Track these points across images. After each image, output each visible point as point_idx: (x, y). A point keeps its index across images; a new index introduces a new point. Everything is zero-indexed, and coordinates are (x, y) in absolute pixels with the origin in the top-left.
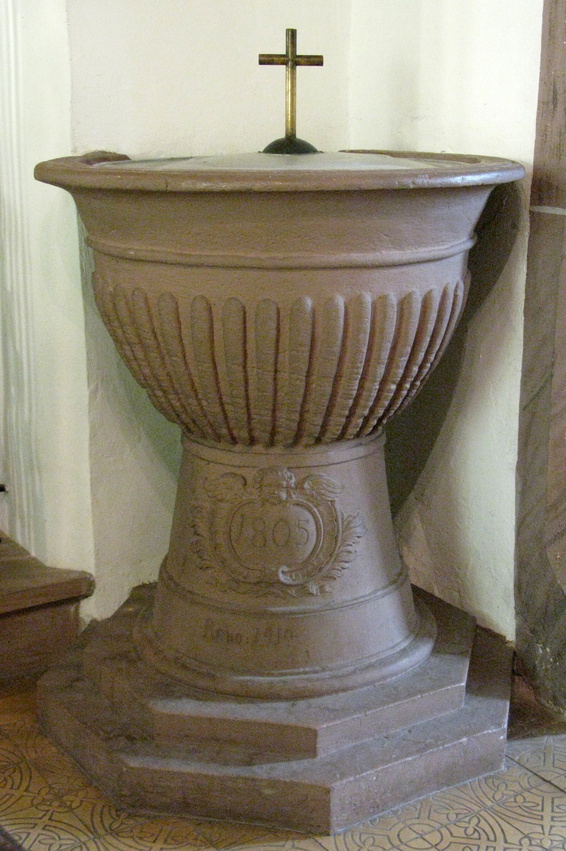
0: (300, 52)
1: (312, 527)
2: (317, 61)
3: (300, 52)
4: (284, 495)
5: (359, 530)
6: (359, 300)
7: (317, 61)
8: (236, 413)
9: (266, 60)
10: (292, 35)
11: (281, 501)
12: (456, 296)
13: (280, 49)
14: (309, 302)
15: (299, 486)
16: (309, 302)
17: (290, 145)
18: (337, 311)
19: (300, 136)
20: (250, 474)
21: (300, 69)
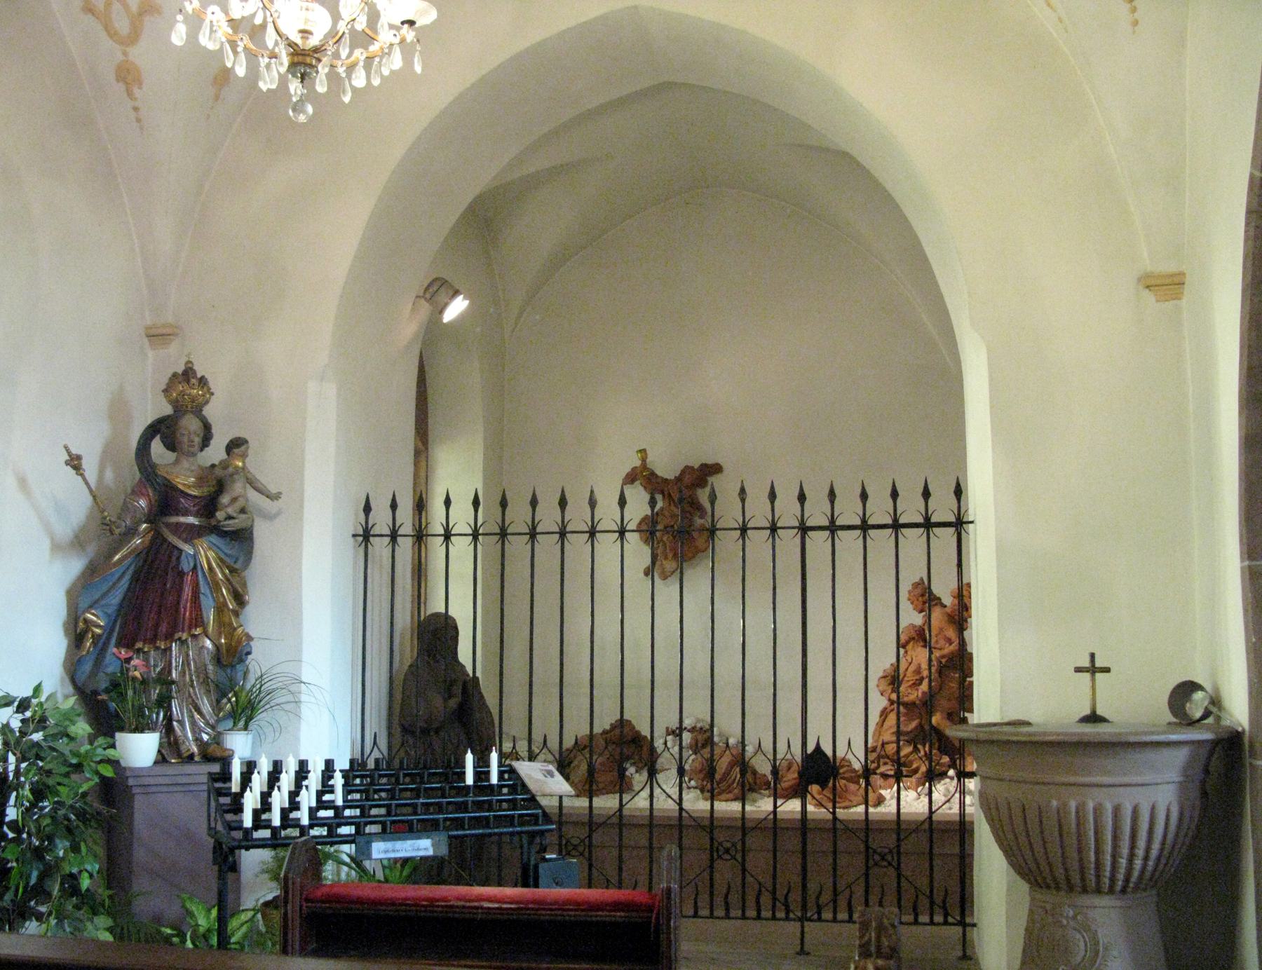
0: (1098, 665)
1: (1082, 944)
2: (1107, 670)
3: (1098, 665)
4: (1065, 922)
5: (1115, 953)
6: (1065, 805)
7: (1107, 670)
8: (1060, 872)
9: (1078, 670)
10: (1092, 656)
11: (1062, 926)
12: (1168, 817)
13: (1087, 664)
14: (1055, 803)
15: (1074, 918)
16: (1055, 803)
17: (1093, 718)
18: (1070, 813)
19: (1099, 712)
20: (1048, 907)
21: (1098, 675)
